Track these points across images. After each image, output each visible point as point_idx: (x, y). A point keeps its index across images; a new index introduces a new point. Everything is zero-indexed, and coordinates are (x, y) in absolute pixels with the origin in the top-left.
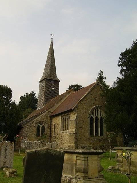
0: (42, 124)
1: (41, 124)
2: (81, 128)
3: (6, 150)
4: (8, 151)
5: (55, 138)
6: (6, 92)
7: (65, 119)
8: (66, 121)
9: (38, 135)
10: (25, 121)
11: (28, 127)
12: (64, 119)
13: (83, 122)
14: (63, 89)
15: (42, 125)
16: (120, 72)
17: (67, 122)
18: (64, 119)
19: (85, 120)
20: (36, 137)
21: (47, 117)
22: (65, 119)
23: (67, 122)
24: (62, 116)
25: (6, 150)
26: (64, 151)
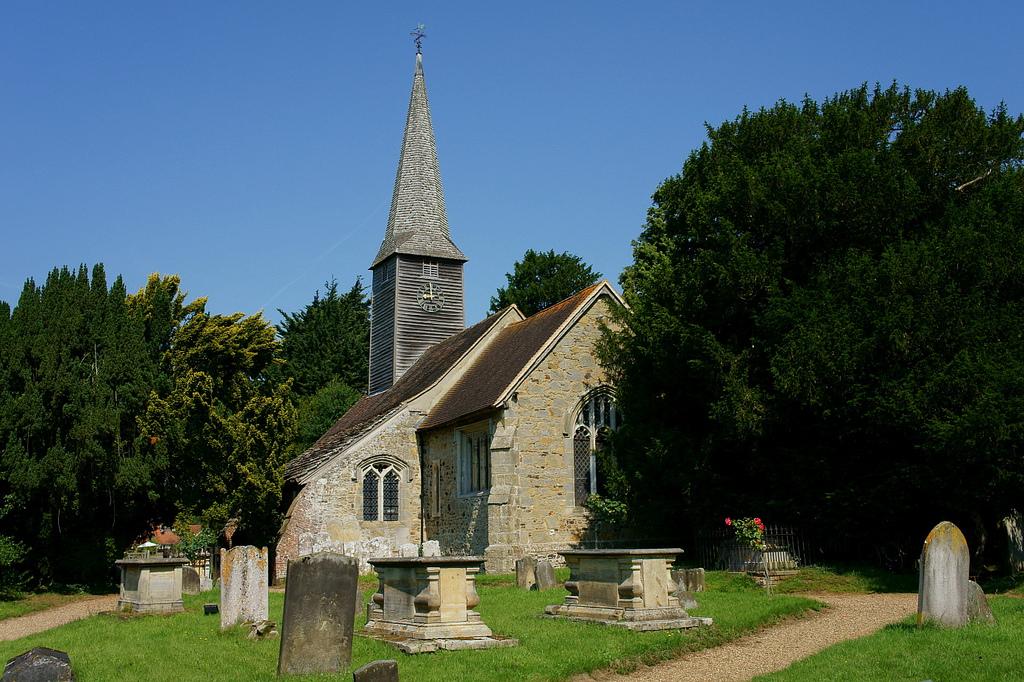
0: (386, 467)
1: (381, 467)
2: (537, 477)
3: (244, 572)
4: (250, 576)
5: (440, 521)
6: (6, 307)
7: (475, 443)
8: (478, 450)
9: (370, 513)
10: (860, 341)
11: (324, 481)
12: (470, 441)
13: (545, 454)
14: (716, 130)
15: (385, 471)
16: (717, 126)
17: (482, 456)
18: (470, 441)
19: (552, 448)
20: (360, 524)
21: (404, 436)
22: (475, 443)
23: (482, 456)
24: (462, 432)
25: (244, 572)
26: (1014, 538)
